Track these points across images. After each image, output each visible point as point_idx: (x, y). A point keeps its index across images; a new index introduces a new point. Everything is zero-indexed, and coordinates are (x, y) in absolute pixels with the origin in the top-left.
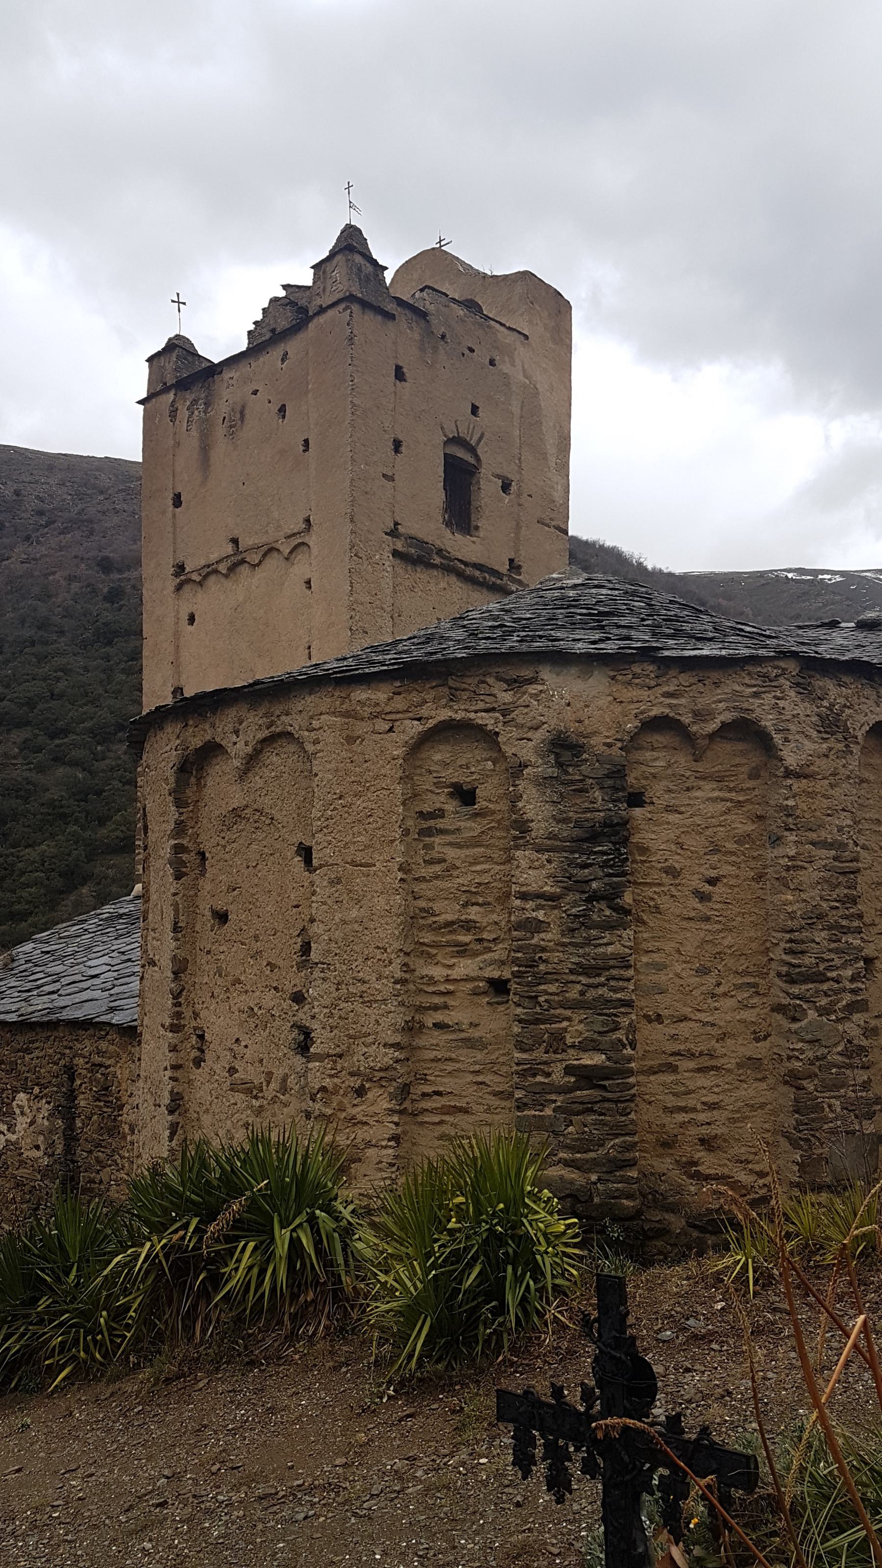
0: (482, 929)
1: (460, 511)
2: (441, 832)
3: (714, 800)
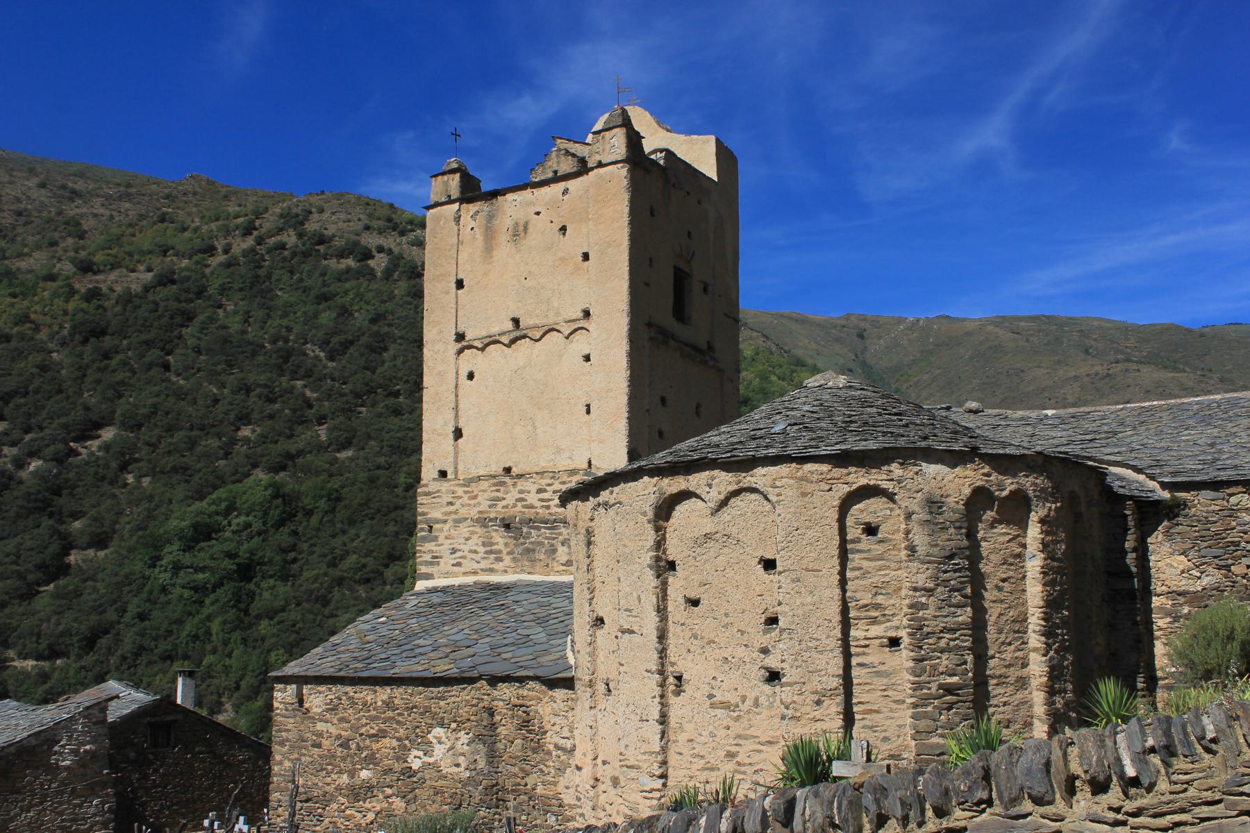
0: (885, 609)
1: (680, 312)
2: (859, 551)
3: (1004, 534)
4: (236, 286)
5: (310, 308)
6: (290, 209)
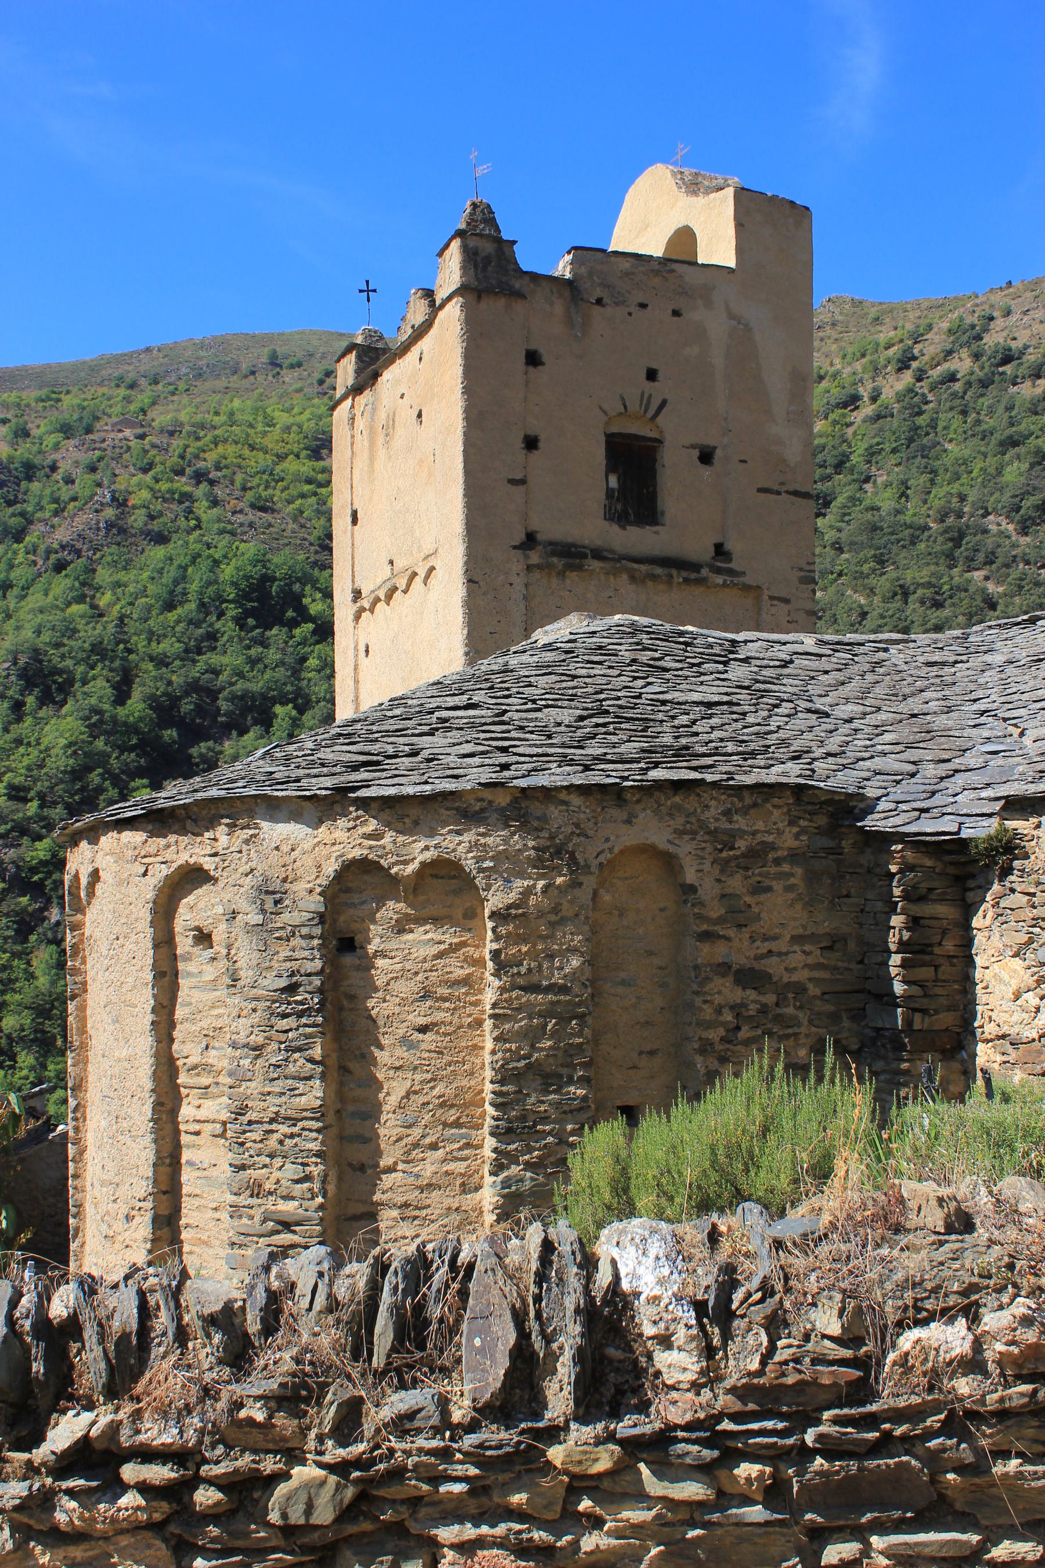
4: (887, 447)
5: (992, 462)
6: (961, 319)
